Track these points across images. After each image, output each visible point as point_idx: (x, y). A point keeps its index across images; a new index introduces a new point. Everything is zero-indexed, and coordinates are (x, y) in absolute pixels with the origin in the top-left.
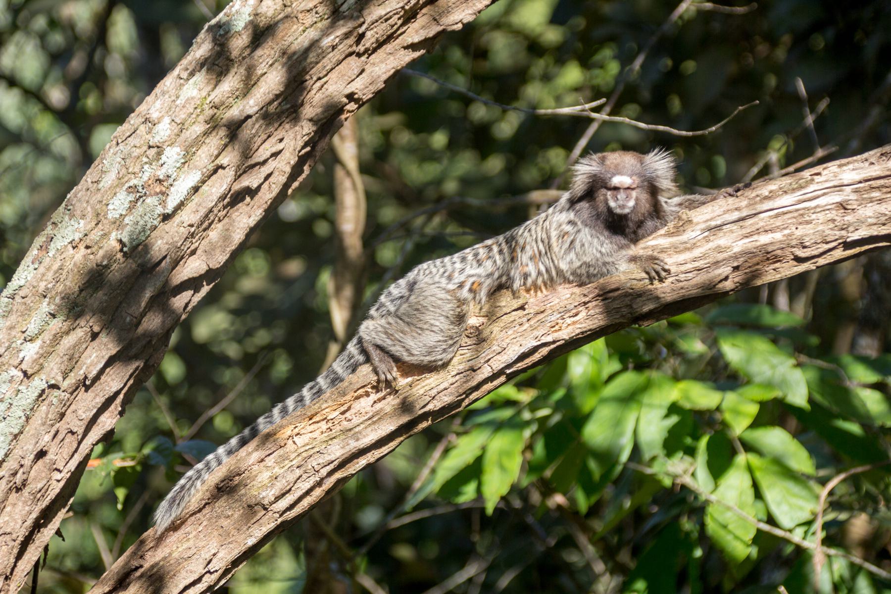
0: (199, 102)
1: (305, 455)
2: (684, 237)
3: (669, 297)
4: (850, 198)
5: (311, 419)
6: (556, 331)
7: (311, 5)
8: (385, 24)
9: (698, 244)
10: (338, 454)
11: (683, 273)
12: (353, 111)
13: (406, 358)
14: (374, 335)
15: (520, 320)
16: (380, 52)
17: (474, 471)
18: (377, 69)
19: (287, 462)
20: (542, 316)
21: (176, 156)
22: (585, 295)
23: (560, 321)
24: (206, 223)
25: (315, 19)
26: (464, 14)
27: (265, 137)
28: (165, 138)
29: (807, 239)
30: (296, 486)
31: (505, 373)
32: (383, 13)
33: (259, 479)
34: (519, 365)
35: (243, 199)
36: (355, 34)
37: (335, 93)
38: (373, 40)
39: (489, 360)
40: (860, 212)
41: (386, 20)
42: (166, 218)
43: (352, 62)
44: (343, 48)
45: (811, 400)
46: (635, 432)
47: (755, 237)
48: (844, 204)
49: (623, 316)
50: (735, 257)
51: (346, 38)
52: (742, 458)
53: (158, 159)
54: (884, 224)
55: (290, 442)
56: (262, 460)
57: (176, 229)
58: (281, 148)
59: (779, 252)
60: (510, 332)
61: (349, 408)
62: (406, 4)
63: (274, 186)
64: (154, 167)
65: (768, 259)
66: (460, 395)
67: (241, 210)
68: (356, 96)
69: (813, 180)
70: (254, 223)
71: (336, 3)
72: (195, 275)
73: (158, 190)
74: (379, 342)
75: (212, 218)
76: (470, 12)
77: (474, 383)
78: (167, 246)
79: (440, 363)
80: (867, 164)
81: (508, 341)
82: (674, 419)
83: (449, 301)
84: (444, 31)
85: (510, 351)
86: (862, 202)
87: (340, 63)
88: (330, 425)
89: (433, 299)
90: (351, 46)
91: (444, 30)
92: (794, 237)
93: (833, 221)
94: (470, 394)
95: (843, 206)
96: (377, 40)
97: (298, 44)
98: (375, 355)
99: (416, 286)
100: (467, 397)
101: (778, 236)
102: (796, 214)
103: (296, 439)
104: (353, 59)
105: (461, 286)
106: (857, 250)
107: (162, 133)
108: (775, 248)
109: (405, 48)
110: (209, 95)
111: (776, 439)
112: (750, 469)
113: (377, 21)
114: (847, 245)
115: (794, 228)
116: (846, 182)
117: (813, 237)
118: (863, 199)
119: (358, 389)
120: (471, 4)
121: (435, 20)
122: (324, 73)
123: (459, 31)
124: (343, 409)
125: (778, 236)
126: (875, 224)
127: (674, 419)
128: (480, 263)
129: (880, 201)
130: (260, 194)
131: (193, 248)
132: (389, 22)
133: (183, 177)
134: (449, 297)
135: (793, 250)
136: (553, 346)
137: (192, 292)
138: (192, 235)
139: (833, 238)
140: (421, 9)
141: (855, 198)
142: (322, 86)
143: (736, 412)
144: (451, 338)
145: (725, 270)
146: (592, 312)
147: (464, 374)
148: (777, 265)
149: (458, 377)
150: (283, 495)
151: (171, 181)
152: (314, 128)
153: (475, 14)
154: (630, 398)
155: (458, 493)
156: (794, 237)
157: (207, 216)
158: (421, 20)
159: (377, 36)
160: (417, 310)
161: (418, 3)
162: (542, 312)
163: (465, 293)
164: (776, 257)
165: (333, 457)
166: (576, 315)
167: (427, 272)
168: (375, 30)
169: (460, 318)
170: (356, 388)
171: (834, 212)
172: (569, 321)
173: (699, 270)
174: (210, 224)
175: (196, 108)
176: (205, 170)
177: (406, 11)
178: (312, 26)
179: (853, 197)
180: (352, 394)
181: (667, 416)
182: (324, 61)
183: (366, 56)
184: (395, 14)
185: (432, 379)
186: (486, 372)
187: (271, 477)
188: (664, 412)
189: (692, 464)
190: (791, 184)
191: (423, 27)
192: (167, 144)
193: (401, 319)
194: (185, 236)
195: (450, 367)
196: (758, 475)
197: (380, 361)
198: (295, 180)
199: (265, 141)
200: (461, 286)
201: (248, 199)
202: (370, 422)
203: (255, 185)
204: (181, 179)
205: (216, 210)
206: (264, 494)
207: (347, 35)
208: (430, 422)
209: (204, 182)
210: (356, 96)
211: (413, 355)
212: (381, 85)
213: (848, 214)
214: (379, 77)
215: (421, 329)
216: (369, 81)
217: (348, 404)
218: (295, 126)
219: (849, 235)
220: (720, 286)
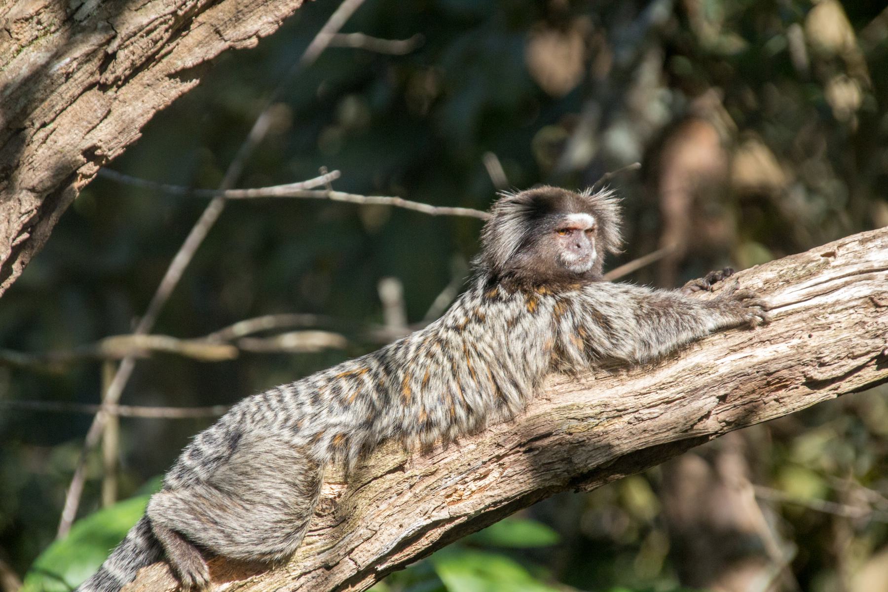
3: (626, 446)
6: (454, 502)
7: (31, 11)
8: (145, 39)
13: (225, 549)
14: (171, 514)
20: (431, 480)
22: (499, 445)
23: (459, 487)
25: (36, 33)
26: (260, 23)
29: (827, 352)
32: (145, 21)
34: (396, 557)
37: (68, 148)
38: (127, 64)
39: (353, 550)
41: (148, 33)
43: (94, 99)
44: (82, 77)
47: (747, 352)
48: (876, 299)
49: (556, 476)
50: (722, 381)
51: (87, 62)
59: (785, 373)
60: (383, 506)
62: (180, 8)
65: (768, 384)
69: (828, 263)
71: (68, 7)
74: (180, 526)
76: (270, 19)
79: (279, 556)
83: (296, 461)
84: (231, 50)
85: (385, 536)
87: (74, 100)
89: (270, 457)
90: (92, 74)
91: (231, 47)
92: (807, 349)
96: (133, 64)
97: (11, 71)
98: (174, 549)
99: (242, 441)
101: (783, 348)
102: (805, 315)
104: (93, 96)
105: (315, 439)
108: (780, 366)
109: (171, 76)
113: (135, 34)
115: (806, 336)
116: (876, 266)
117: (835, 349)
120: (271, 7)
121: (217, 32)
122: (52, 116)
123: (253, 49)
125: (783, 348)
128: (345, 406)
132: (153, 35)
134: (297, 455)
135: (806, 369)
136: (448, 527)
140: (197, 15)
142: (47, 137)
144: (300, 517)
145: (708, 402)
146: (509, 471)
147: (313, 574)
148: (782, 393)
149: (303, 580)
152: (38, 203)
153: (277, 22)
156: (807, 349)
158: (197, 33)
159: (132, 57)
160: (242, 474)
161: (195, 6)
162: (433, 474)
163: (321, 451)
164: (781, 380)
166: (485, 476)
167: (258, 417)
168: (131, 48)
169: (312, 487)
171: (861, 311)
172: (473, 486)
173: (668, 403)
178: (31, 43)
182: (52, 97)
184: (161, 23)
185: (262, 584)
186: (347, 570)
190: (795, 270)
191: (199, 44)
193: (216, 488)
195: (291, 565)
197: (183, 555)
200: (315, 439)
207: (88, 57)
210: (98, 152)
211: (237, 544)
212: (136, 135)
214: (133, 121)
215: (252, 503)
216: (118, 128)
220: (700, 426)
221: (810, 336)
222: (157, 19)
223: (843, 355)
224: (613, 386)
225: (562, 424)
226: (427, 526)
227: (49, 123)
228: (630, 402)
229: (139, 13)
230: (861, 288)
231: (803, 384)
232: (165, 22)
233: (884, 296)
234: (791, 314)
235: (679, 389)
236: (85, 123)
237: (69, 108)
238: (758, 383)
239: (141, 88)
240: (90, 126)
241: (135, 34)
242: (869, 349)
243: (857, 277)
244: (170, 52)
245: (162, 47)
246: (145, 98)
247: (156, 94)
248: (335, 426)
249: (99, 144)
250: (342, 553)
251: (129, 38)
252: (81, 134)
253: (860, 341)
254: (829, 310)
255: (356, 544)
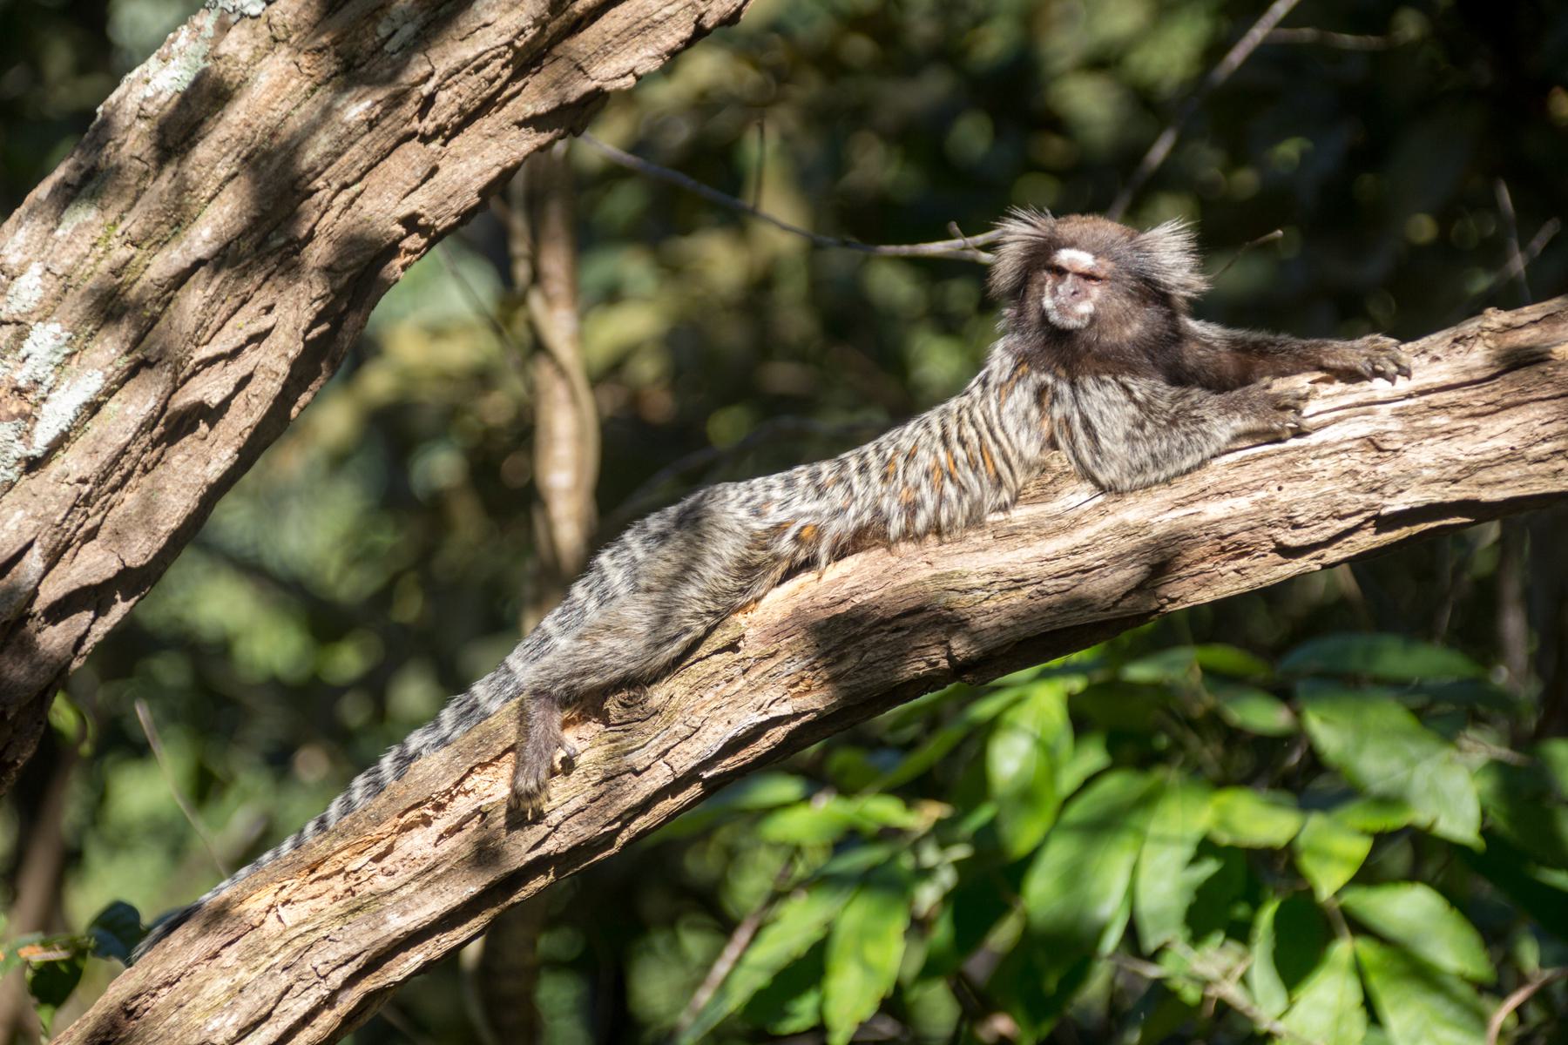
0: (100, 233)
1: (298, 943)
2: (1056, 506)
4: (1388, 428)
5: (313, 871)
6: (800, 694)
8: (475, 77)
9: (1085, 519)
10: (365, 942)
11: (1051, 577)
12: (417, 251)
15: (729, 672)
16: (471, 135)
17: (808, 969)
18: (464, 166)
19: (263, 958)
20: (771, 663)
21: (51, 342)
24: (116, 477)
26: (638, 57)
27: (236, 302)
28: (32, 305)
30: (281, 1008)
31: (700, 779)
32: (470, 54)
33: (208, 992)
34: (728, 761)
35: (193, 428)
36: (415, 97)
38: (453, 108)
39: (667, 751)
40: (1409, 456)
41: (478, 69)
42: (33, 465)
45: (1485, 832)
46: (1131, 894)
47: (1199, 506)
48: (1376, 440)
52: (1343, 949)
53: (18, 348)
54: (1455, 481)
55: (272, 917)
56: (216, 955)
57: (52, 488)
58: (269, 324)
59: (1245, 537)
60: (709, 696)
61: (389, 850)
62: (517, 37)
63: (255, 401)
64: (11, 364)
65: (1223, 550)
66: (610, 823)
67: (189, 450)
68: (422, 221)
70: (218, 475)
72: (95, 580)
73: (14, 409)
75: (128, 466)
76: (651, 53)
77: (635, 798)
78: (34, 523)
80: (1425, 359)
81: (703, 713)
82: (1209, 867)
85: (709, 735)
86: (1415, 436)
88: (352, 882)
91: (598, 88)
92: (1274, 506)
93: (1354, 473)
94: (632, 820)
95: (1373, 444)
96: (461, 110)
100: (624, 826)
101: (1243, 504)
102: (1280, 460)
103: (282, 911)
104: (413, 149)
105: (780, 529)
106: (1403, 532)
107: (25, 295)
109: (522, 124)
110: (122, 219)
111: (1409, 908)
112: (1359, 970)
113: (458, 71)
114: (1384, 523)
115: (1274, 488)
116: (1380, 397)
117: (1313, 506)
118: (1415, 430)
119: (407, 811)
120: (651, 37)
122: (355, 174)
124: (376, 850)
125: (1243, 504)
126: (1437, 481)
127: (1209, 867)
129: (1450, 434)
130: (228, 417)
131: (89, 525)
132: (485, 72)
133: (67, 383)
135: (1273, 531)
136: (794, 725)
137: (91, 615)
138: (87, 500)
139: (1353, 508)
141: (1399, 428)
142: (352, 201)
143: (1325, 856)
148: (1243, 562)
150: (255, 1025)
151: (42, 390)
153: (660, 56)
154: (1104, 827)
155: (784, 1015)
156: (1274, 506)
157: (115, 461)
159: (459, 100)
162: (772, 656)
164: (1239, 545)
165: (353, 949)
168: (456, 88)
170: (401, 808)
171: (1357, 456)
173: (1084, 572)
174: (125, 479)
175: (94, 245)
176: (110, 370)
177: (517, 51)
179: (1395, 425)
180: (395, 820)
181: (1195, 860)
183: (440, 140)
184: (494, 57)
187: (230, 988)
188: (1187, 851)
189: (1242, 958)
192: (36, 316)
194: (70, 503)
196: (1375, 981)
198: (304, 389)
199: (235, 311)
201: (203, 427)
202: (429, 877)
203: (215, 399)
204: (63, 388)
205: (135, 450)
206: (216, 1023)
208: (551, 877)
209: (110, 393)
210: (422, 221)
213: (1385, 460)
214: (468, 182)
217: (388, 841)
218: (297, 280)
219: (1386, 501)
221: (1280, 489)
222: (486, 51)
223: (1325, 515)
224: (1016, 548)
225: (938, 597)
226: (763, 723)
227: (353, 183)
228: (1033, 570)
229: (465, 43)
230: (1357, 426)
231: (1272, 551)
232: (499, 56)
233: (1388, 436)
234: (1261, 458)
235: (1097, 555)
236: (400, 184)
237: (381, 165)
238: (1209, 549)
239: (480, 140)
240: (408, 188)
241: (458, 71)
242: (1361, 506)
243: (1352, 411)
244: (518, 93)
245: (504, 87)
246: (487, 152)
247: (501, 147)
248: (806, 515)
249: (421, 211)
250: (652, 755)
251: (450, 76)
252: (396, 198)
253: (1349, 496)
254: (1312, 454)
255: (671, 743)
